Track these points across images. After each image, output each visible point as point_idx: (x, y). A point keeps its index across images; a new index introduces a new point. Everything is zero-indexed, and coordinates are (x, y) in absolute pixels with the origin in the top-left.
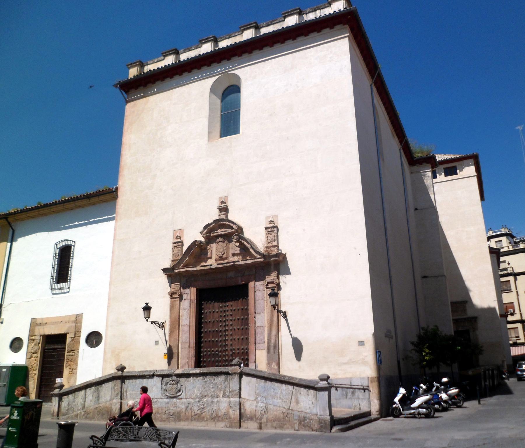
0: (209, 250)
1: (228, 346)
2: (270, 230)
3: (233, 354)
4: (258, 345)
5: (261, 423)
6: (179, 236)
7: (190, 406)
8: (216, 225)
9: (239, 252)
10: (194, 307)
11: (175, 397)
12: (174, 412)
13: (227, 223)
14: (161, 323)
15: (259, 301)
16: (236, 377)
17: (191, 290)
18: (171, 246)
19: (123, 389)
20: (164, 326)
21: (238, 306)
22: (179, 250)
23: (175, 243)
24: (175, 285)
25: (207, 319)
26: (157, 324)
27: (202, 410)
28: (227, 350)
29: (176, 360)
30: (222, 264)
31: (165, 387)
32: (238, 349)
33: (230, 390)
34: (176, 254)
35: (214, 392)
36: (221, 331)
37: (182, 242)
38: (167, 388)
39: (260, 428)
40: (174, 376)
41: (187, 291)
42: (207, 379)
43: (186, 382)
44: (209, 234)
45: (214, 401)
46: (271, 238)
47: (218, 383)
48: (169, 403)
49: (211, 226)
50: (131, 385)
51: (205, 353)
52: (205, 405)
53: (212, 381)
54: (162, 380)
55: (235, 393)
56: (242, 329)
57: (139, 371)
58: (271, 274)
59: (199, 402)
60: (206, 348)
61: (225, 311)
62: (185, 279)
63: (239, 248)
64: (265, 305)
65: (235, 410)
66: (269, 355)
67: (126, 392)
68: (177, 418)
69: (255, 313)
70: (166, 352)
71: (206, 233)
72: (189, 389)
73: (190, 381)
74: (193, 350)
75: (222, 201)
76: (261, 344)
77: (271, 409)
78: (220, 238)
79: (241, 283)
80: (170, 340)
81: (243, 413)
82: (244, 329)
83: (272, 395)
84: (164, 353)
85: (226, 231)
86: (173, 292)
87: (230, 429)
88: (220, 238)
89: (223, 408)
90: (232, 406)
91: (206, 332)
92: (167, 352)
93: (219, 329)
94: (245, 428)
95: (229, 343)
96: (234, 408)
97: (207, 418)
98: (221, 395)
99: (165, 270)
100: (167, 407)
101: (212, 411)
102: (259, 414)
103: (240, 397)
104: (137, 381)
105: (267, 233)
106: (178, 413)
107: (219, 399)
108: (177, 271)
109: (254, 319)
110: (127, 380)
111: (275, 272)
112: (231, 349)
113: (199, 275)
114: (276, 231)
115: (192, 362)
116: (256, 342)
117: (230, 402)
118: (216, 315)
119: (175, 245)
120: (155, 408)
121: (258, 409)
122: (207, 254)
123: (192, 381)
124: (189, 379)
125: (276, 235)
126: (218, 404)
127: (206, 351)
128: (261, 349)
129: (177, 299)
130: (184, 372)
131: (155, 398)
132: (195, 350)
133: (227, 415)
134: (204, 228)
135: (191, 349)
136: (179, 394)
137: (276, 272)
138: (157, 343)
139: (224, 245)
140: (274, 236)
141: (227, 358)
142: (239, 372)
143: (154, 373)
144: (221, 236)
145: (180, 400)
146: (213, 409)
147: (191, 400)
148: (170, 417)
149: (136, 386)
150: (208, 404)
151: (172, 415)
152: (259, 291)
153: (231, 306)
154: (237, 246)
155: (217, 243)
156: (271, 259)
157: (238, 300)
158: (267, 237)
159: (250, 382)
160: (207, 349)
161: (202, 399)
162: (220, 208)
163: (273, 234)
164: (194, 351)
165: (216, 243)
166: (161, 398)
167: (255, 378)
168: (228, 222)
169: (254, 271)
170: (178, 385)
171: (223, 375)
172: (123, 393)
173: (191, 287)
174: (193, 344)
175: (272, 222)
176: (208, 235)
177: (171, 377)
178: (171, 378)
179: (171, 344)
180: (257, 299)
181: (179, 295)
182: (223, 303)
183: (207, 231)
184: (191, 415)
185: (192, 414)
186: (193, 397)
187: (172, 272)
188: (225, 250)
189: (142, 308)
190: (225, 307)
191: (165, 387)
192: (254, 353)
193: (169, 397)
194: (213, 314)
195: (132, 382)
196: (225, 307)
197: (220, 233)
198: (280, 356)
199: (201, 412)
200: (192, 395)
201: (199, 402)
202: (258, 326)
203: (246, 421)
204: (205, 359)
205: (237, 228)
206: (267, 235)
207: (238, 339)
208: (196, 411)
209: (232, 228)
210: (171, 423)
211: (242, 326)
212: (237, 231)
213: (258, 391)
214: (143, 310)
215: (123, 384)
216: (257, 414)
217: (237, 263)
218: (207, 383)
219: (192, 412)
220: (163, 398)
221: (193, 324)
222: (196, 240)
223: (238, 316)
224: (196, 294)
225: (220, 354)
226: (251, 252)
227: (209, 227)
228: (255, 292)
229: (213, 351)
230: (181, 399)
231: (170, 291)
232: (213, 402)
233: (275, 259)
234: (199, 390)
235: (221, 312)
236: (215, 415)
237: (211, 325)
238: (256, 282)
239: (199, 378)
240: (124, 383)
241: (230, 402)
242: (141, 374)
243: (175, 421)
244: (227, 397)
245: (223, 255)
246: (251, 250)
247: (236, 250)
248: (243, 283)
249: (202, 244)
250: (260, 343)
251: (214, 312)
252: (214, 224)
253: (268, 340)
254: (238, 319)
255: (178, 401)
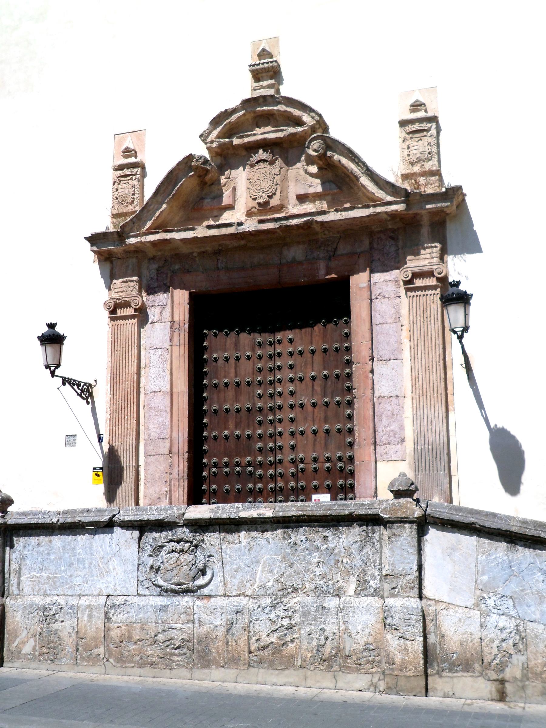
0: (225, 185)
1: (284, 450)
2: (416, 127)
3: (300, 474)
4: (384, 447)
5: (502, 682)
6: (133, 150)
7: (242, 621)
8: (247, 117)
9: (319, 189)
10: (182, 341)
11: (186, 591)
12: (185, 637)
13: (282, 110)
14: (85, 384)
15: (384, 325)
16: (408, 530)
17: (172, 297)
18: (111, 175)
19: (7, 564)
20: (91, 395)
21: (312, 344)
22: (134, 186)
23: (121, 168)
24: (123, 282)
25: (217, 378)
26: (75, 387)
27: (286, 635)
28: (281, 462)
29: (133, 486)
30: (275, 220)
31: (150, 561)
32: (315, 460)
33: (384, 573)
34: (125, 197)
35: (324, 576)
36: (260, 410)
37: (141, 166)
38: (158, 564)
39: (502, 697)
40: (182, 526)
41: (161, 298)
42: (298, 537)
43: (224, 547)
44: (227, 140)
45: (325, 605)
46: (421, 150)
47: (340, 552)
48: (166, 611)
49: (234, 117)
50: (35, 553)
51: (214, 470)
52: (297, 618)
53: (319, 543)
54: (140, 539)
55: (402, 581)
56: (327, 404)
57: (61, 510)
58: (422, 252)
59: (274, 607)
60: (215, 456)
61: (271, 357)
62: (154, 266)
63: (319, 181)
64: (402, 337)
65: (407, 635)
66: (420, 476)
67: (19, 573)
68: (195, 656)
69: (373, 359)
70: (99, 463)
71: (218, 137)
72: (235, 567)
73: (240, 542)
74: (181, 461)
75: (264, 50)
76: (392, 446)
77: (536, 637)
78: (261, 151)
79: (326, 277)
80: (112, 432)
81: (434, 644)
82: (330, 406)
83: (538, 593)
84: (94, 469)
85: (282, 131)
86: (118, 301)
87: (393, 698)
88: (261, 151)
89: (359, 628)
90: (394, 622)
91: (215, 411)
92: (103, 465)
93: (254, 404)
94: (445, 696)
95: (286, 441)
96: (403, 629)
97: (304, 660)
98: (351, 588)
99: (94, 239)
100: (160, 621)
101: (322, 638)
102: (495, 651)
103: (421, 597)
104: (54, 542)
105: (406, 135)
106: (199, 642)
107: (343, 598)
108: (132, 241)
109: (371, 375)
110: (21, 539)
111: (433, 245)
112: (292, 459)
113: (195, 254)
114: (433, 131)
115: (182, 492)
116: (377, 440)
117: (386, 612)
118: (246, 367)
119: (119, 173)
120: (120, 625)
121: (490, 636)
122: (221, 196)
123: (244, 542)
124: (236, 536)
125: (433, 141)
126: (343, 617)
127: (215, 465)
128: (394, 459)
129: (130, 321)
130: (218, 515)
131: (115, 593)
132: (189, 459)
133: (376, 653)
134: (211, 123)
135: (176, 458)
136: (201, 581)
137: (438, 245)
138: (70, 440)
139: (274, 172)
140: (429, 144)
141: (280, 484)
142: (415, 516)
143: (114, 516)
144: (265, 145)
145: (205, 601)
146: (323, 630)
147: (244, 601)
148: (172, 654)
149: (52, 557)
150: (305, 614)
151: (178, 648)
152: (384, 297)
153: (291, 341)
154: (312, 175)
155: (252, 166)
156: (428, 207)
157: (313, 327)
158: (408, 148)
159: (454, 549)
160: (220, 459)
161: (285, 600)
162: (258, 67)
163: (426, 140)
164: (186, 464)
165: (248, 167)
166: (139, 595)
167: (471, 535)
168: (287, 106)
169: (367, 242)
170: (198, 553)
171: (355, 525)
172: (6, 576)
173: (175, 288)
174: (181, 445)
175: (420, 105)
176: (225, 144)
177: (171, 530)
178: (170, 533)
179: (116, 444)
180: (377, 319)
181: (136, 310)
182: (267, 334)
183: (220, 132)
184: (246, 649)
185: (249, 647)
186: (249, 593)
187: (118, 245)
188: (277, 184)
189: (38, 338)
190: (271, 344)
191: (150, 561)
192: (373, 470)
193: (166, 591)
194: (236, 364)
195: (39, 545)
196: (271, 344)
197: (260, 137)
198: (454, 480)
199: (279, 638)
200: (248, 585)
201: (274, 607)
202: (382, 395)
203: (444, 674)
204: (214, 487)
205: (314, 122)
206: (407, 143)
207: (315, 432)
208: (263, 637)
209: (299, 122)
210: (174, 671)
211: (325, 396)
212: (313, 129)
213: (485, 578)
214: (39, 342)
215: (8, 549)
216: (486, 650)
217: (320, 218)
218: (299, 549)
219: (249, 639)
220: (147, 592)
221: (182, 389)
222: (191, 155)
223: (313, 370)
224: (187, 307)
225: (260, 472)
226: (363, 186)
227: (228, 121)
228: (371, 300)
229: (238, 464)
230: (209, 596)
231: (108, 299)
232: (324, 608)
233: (439, 205)
234: (271, 572)
235: (260, 357)
236: (334, 652)
237: (231, 393)
238: (372, 275)
239: (269, 534)
240: (12, 546)
241: (386, 612)
242: (69, 520)
243: (191, 665)
244: (372, 595)
245: (270, 197)
246: (365, 181)
247: (310, 186)
248: (333, 276)
249: (209, 168)
250: (389, 444)
251: (238, 359)
252: (242, 113)
253: (415, 432)
254: (313, 378)
255: (198, 603)
